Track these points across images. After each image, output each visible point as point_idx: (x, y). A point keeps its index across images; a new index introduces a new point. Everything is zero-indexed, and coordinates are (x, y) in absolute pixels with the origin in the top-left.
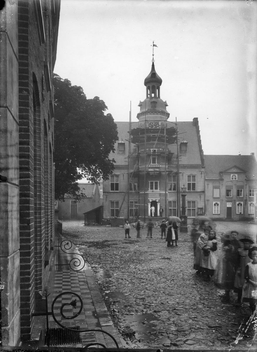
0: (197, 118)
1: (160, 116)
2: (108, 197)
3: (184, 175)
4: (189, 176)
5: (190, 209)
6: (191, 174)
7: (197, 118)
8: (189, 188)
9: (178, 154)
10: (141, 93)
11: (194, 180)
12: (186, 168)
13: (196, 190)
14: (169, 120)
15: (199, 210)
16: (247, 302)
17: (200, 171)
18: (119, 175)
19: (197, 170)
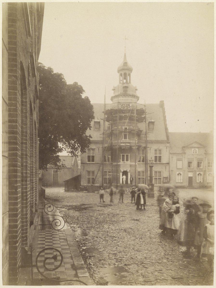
6: (157, 149)
11: (160, 153)
18: (95, 149)
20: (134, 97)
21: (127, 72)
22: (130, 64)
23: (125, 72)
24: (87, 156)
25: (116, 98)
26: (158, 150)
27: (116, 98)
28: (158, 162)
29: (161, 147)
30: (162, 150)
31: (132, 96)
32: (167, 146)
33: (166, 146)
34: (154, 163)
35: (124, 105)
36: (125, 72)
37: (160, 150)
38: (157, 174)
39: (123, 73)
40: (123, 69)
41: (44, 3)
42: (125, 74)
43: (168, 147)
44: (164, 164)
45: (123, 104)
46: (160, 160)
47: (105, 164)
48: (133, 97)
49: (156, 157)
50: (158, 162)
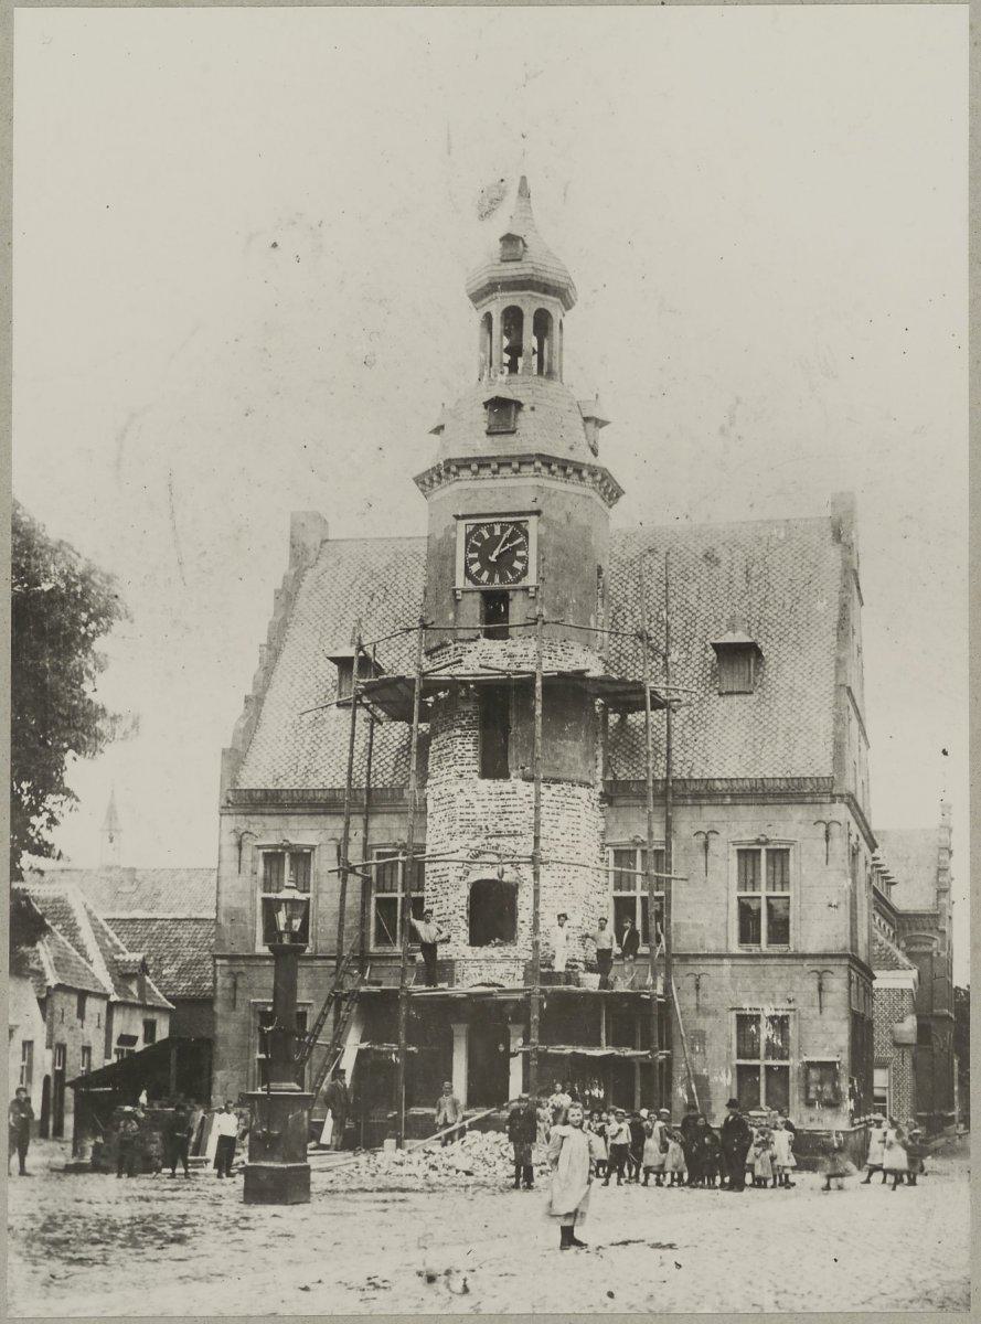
0: (419, 480)
1: (533, 481)
2: (240, 984)
3: (712, 846)
4: (748, 856)
5: (757, 1068)
6: (758, 842)
7: (419, 480)
8: (748, 933)
9: (705, 793)
10: (455, 358)
11: (780, 876)
12: (728, 800)
13: (791, 944)
14: (622, 517)
15: (814, 1075)
16: (872, 1076)
17: (820, 821)
18: (313, 848)
19: (798, 813)
20: (579, 472)
21: (529, 304)
22: (557, 246)
23: (523, 313)
24: (259, 903)
25: (439, 483)
26: (763, 853)
27: (439, 483)
28: (764, 947)
29: (790, 825)
30: (791, 853)
31: (538, 464)
32: (828, 826)
33: (826, 817)
34: (735, 948)
35: (491, 531)
36: (523, 313)
37: (780, 856)
38: (756, 868)
39: (497, 306)
40: (492, 288)
41: (470, 296)
42: (513, 317)
43: (835, 829)
44: (804, 956)
45: (479, 526)
46: (780, 930)
47: (196, 1174)
48: (569, 471)
49: (747, 915)
50: (764, 947)
